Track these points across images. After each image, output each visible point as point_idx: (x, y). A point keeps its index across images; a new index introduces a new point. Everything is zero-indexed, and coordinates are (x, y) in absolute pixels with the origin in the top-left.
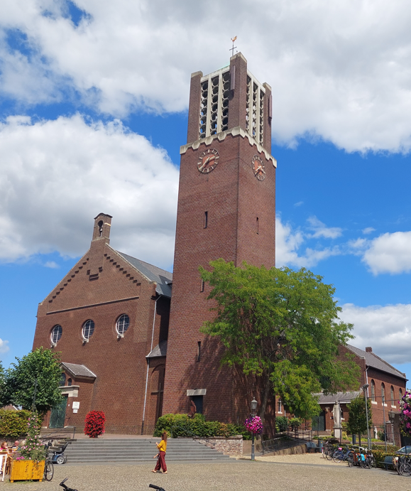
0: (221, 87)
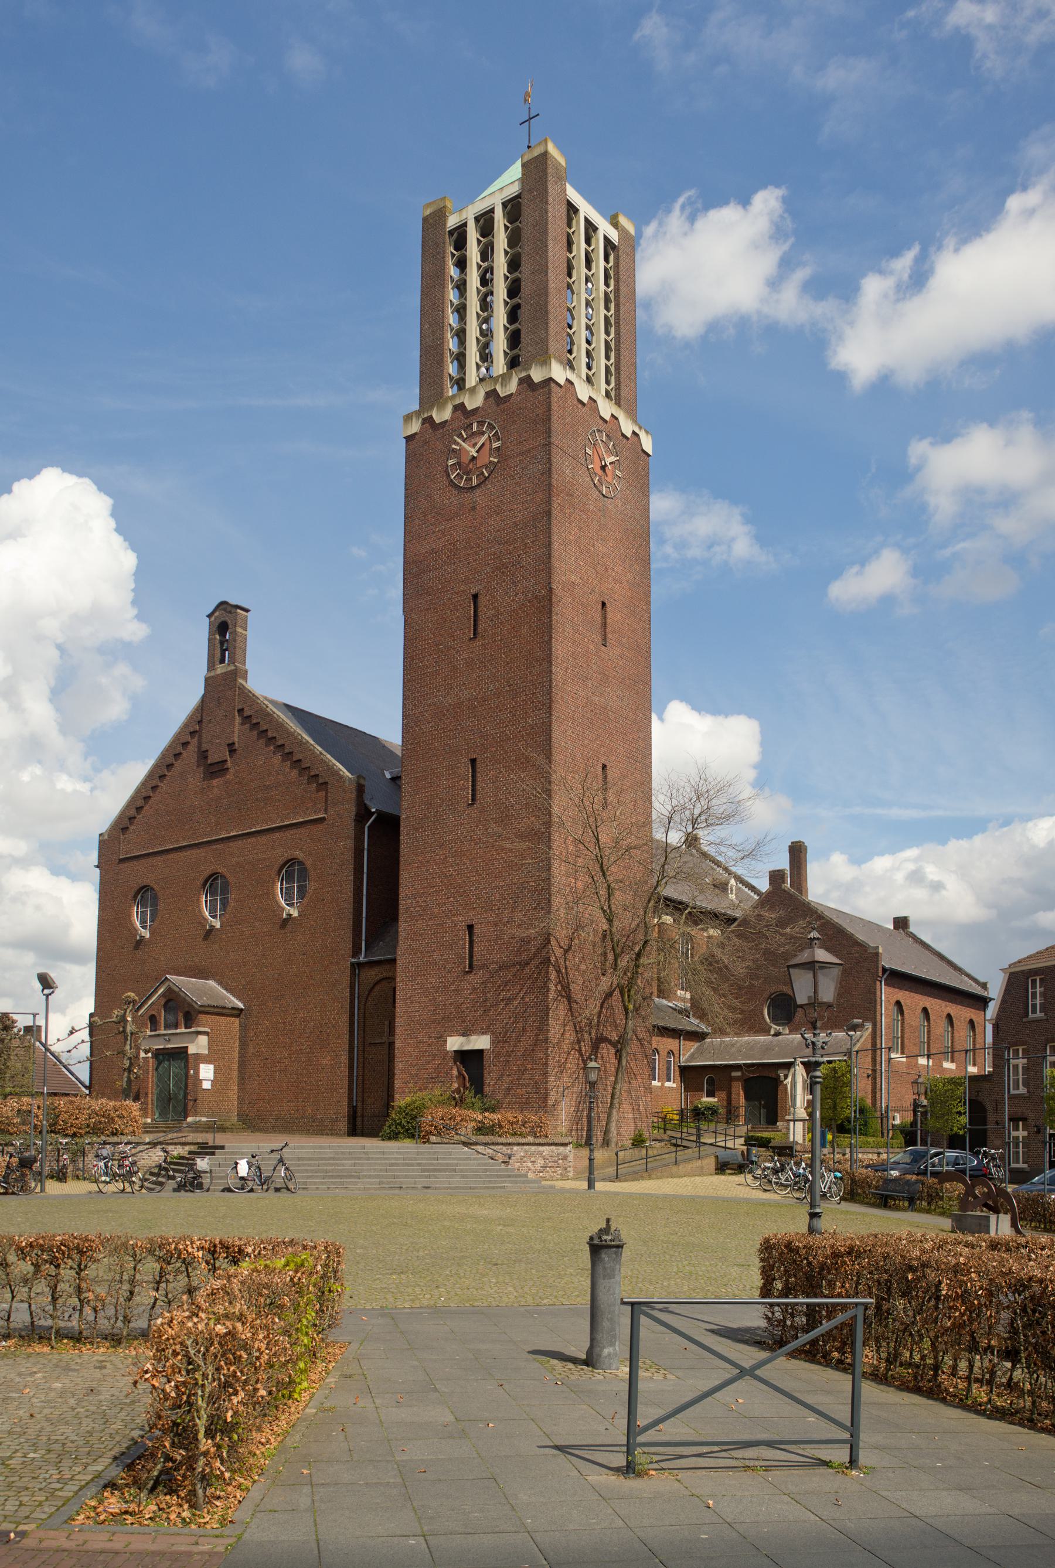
0: (501, 240)
